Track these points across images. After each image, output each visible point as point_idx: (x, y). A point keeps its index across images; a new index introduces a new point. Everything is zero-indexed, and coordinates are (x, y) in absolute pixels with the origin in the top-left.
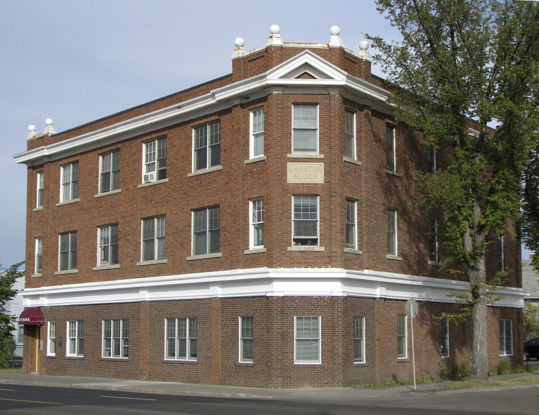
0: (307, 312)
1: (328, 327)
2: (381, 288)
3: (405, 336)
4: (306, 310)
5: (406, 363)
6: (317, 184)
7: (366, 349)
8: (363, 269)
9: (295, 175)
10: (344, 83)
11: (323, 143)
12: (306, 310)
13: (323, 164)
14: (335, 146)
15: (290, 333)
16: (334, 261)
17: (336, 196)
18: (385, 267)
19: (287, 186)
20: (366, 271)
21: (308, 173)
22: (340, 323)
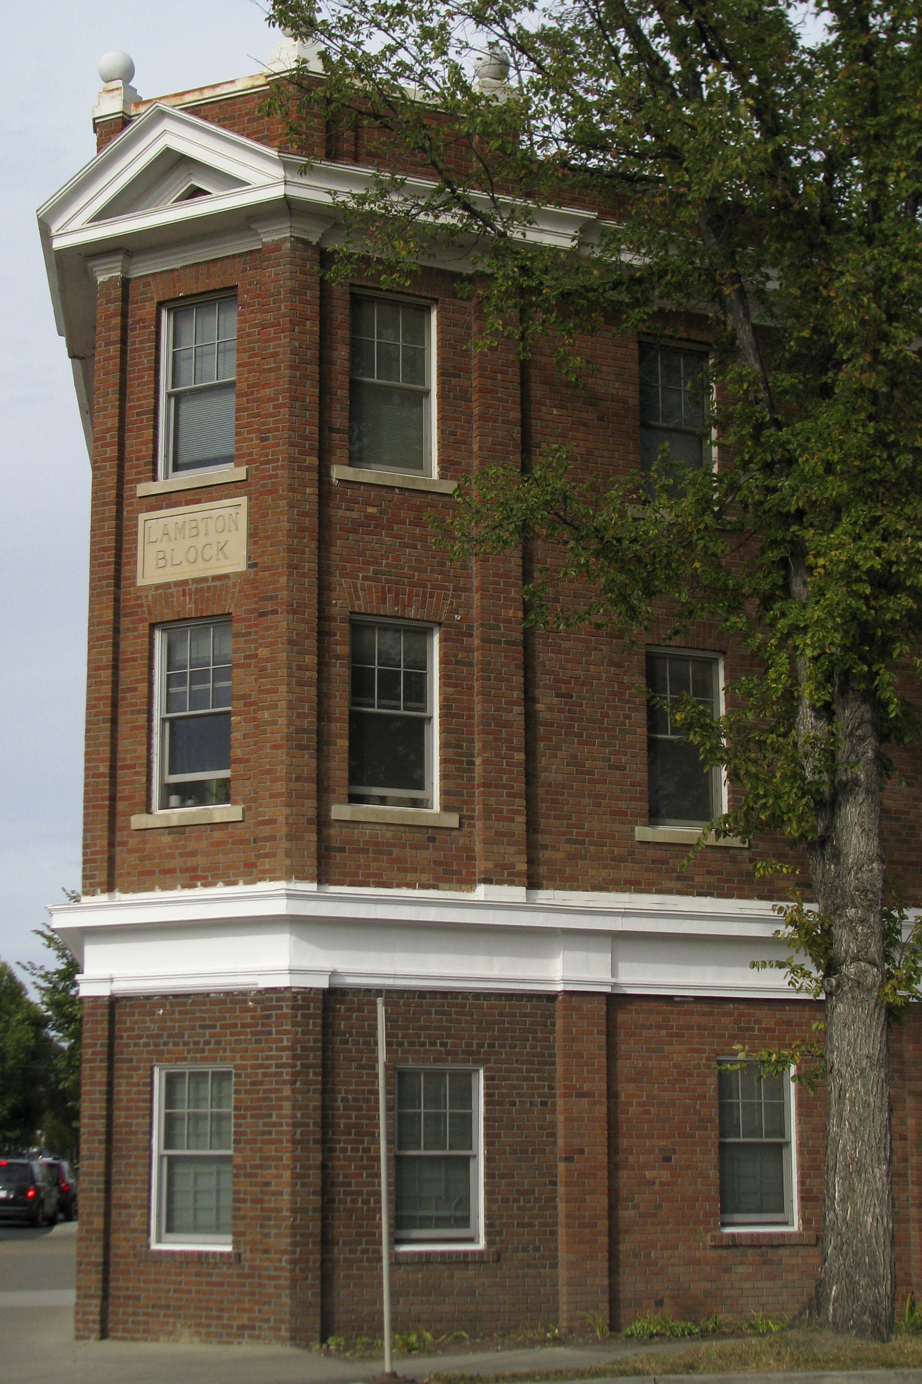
0: (189, 1052)
1: (254, 1108)
2: (569, 954)
3: (788, 1144)
4: (186, 1044)
5: (782, 1252)
6: (226, 577)
7: (487, 1193)
8: (469, 882)
9: (161, 555)
10: (278, 192)
11: (249, 424)
12: (186, 1044)
13: (243, 500)
14: (277, 429)
15: (136, 1133)
16: (267, 855)
17: (275, 612)
18: (627, 875)
19: (137, 598)
20: (481, 892)
21: (201, 540)
22: (287, 1091)
